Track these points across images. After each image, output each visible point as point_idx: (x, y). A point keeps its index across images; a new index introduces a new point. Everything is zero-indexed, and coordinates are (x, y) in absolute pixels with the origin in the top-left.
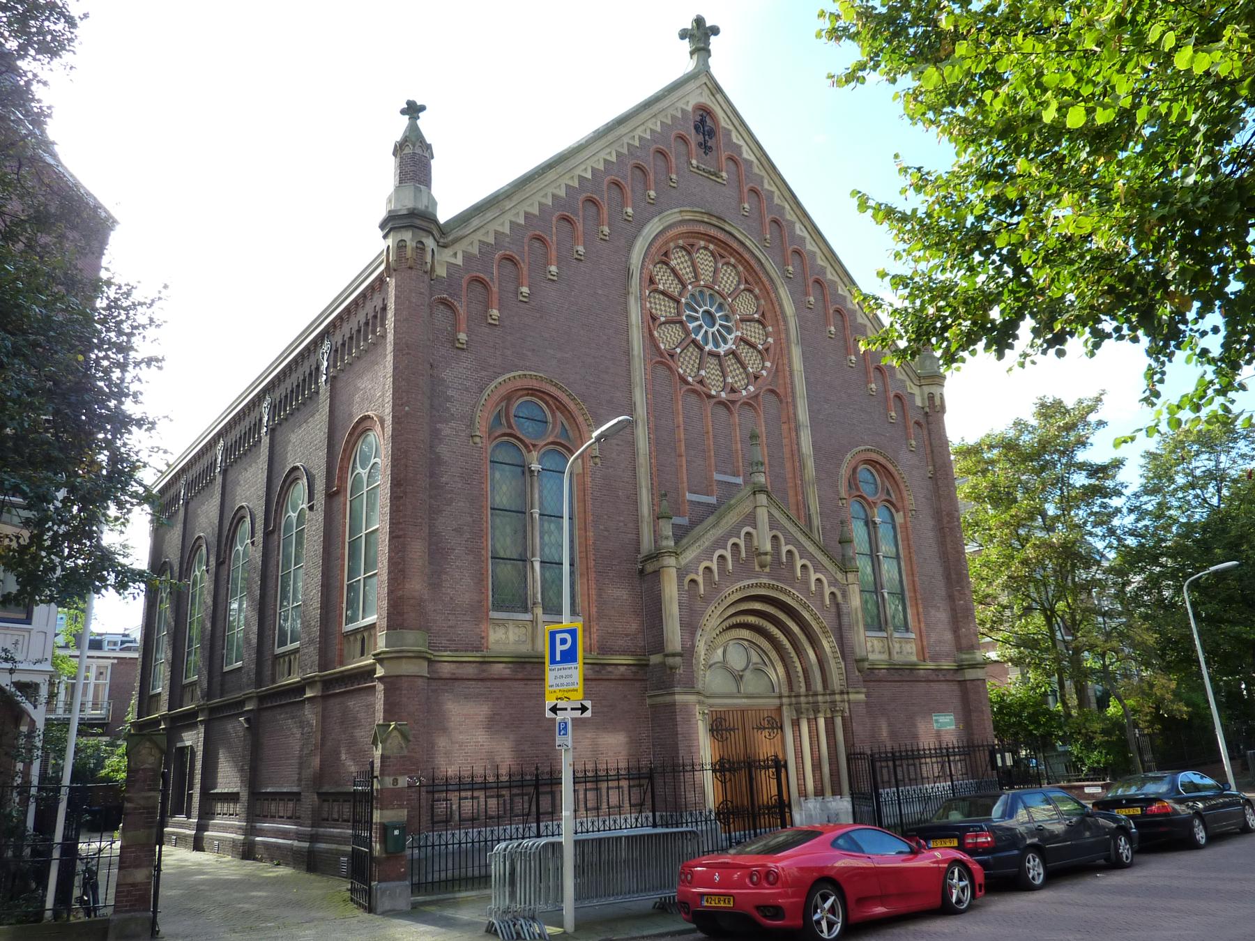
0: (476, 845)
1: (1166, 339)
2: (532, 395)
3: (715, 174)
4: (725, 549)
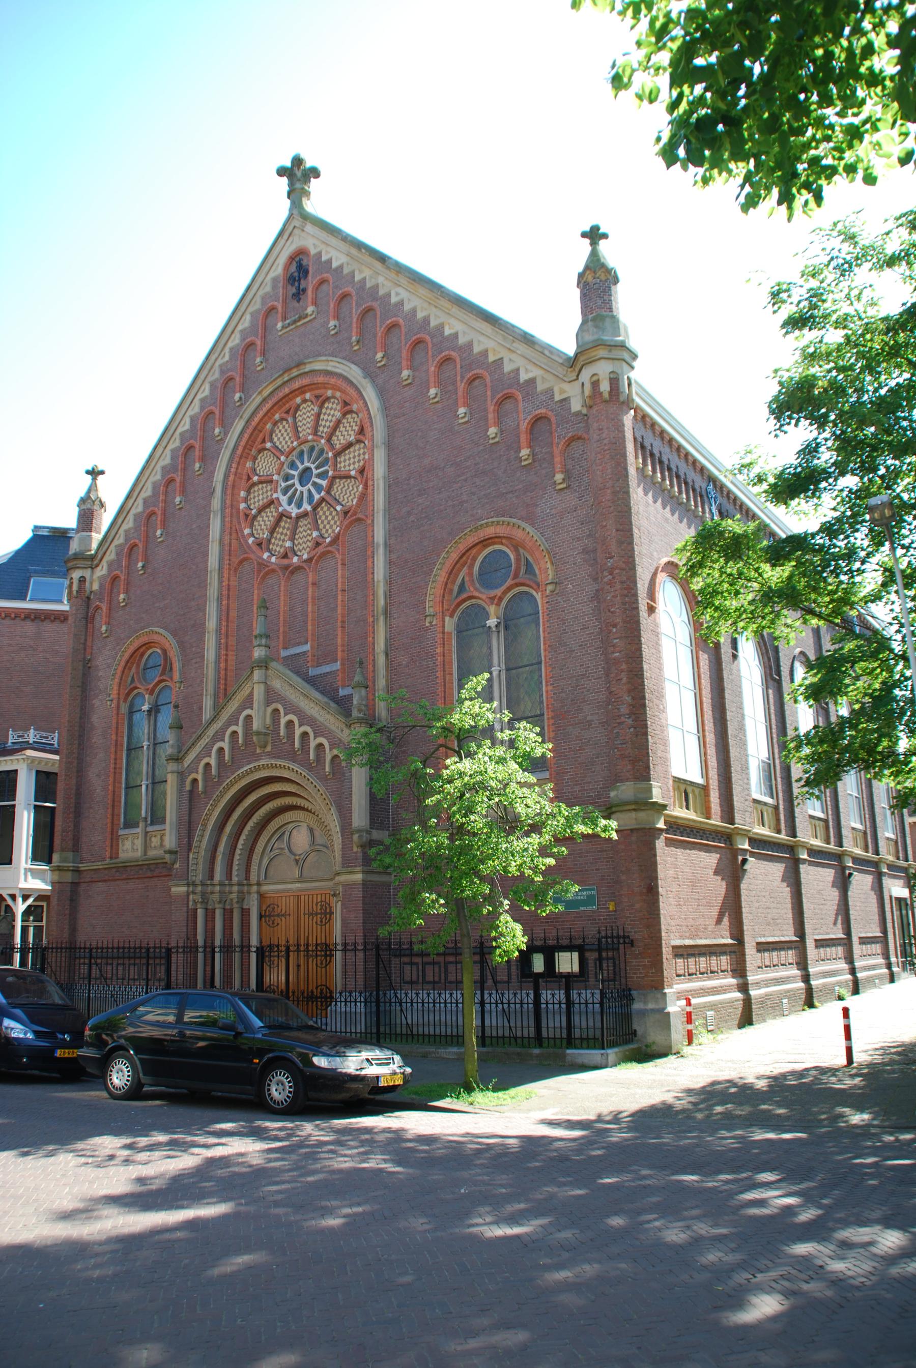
0: (550, 1006)
1: (870, 69)
2: (486, 546)
3: (300, 319)
4: (223, 740)
